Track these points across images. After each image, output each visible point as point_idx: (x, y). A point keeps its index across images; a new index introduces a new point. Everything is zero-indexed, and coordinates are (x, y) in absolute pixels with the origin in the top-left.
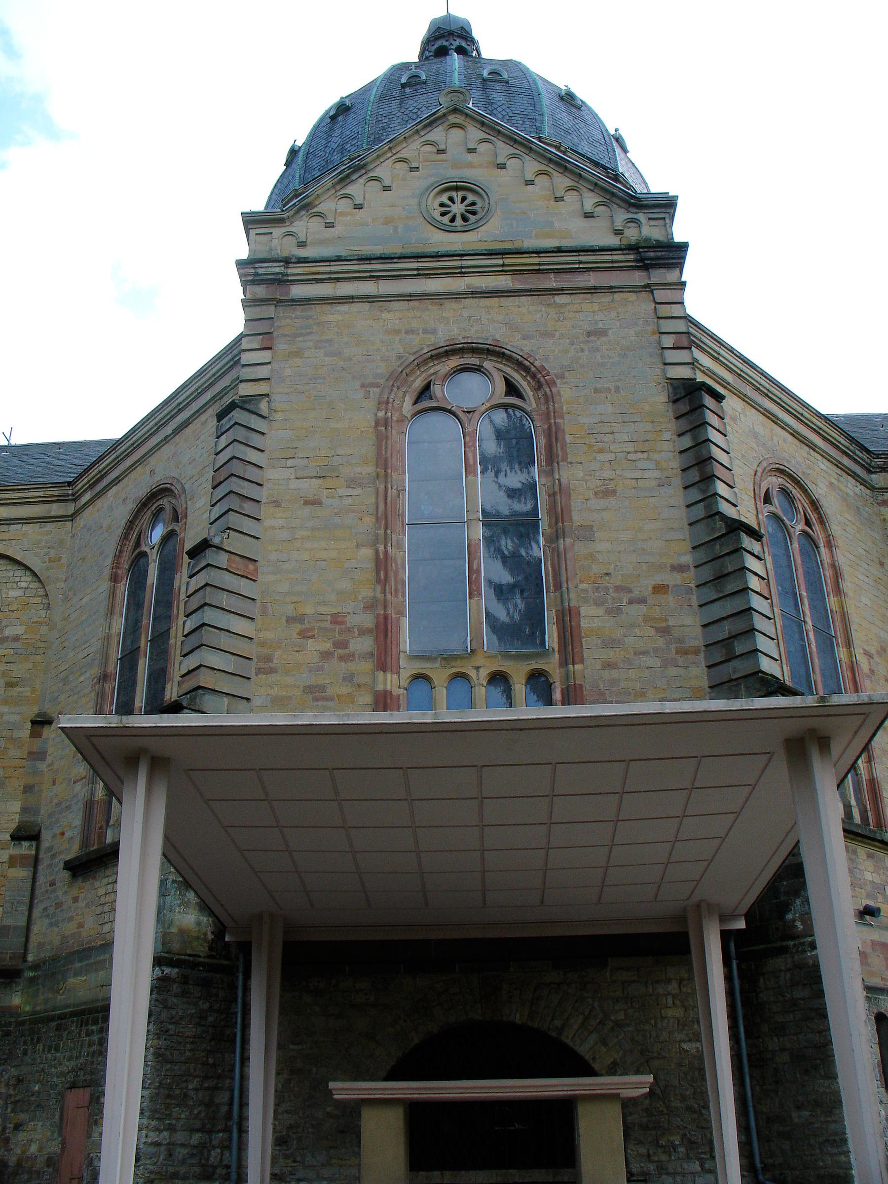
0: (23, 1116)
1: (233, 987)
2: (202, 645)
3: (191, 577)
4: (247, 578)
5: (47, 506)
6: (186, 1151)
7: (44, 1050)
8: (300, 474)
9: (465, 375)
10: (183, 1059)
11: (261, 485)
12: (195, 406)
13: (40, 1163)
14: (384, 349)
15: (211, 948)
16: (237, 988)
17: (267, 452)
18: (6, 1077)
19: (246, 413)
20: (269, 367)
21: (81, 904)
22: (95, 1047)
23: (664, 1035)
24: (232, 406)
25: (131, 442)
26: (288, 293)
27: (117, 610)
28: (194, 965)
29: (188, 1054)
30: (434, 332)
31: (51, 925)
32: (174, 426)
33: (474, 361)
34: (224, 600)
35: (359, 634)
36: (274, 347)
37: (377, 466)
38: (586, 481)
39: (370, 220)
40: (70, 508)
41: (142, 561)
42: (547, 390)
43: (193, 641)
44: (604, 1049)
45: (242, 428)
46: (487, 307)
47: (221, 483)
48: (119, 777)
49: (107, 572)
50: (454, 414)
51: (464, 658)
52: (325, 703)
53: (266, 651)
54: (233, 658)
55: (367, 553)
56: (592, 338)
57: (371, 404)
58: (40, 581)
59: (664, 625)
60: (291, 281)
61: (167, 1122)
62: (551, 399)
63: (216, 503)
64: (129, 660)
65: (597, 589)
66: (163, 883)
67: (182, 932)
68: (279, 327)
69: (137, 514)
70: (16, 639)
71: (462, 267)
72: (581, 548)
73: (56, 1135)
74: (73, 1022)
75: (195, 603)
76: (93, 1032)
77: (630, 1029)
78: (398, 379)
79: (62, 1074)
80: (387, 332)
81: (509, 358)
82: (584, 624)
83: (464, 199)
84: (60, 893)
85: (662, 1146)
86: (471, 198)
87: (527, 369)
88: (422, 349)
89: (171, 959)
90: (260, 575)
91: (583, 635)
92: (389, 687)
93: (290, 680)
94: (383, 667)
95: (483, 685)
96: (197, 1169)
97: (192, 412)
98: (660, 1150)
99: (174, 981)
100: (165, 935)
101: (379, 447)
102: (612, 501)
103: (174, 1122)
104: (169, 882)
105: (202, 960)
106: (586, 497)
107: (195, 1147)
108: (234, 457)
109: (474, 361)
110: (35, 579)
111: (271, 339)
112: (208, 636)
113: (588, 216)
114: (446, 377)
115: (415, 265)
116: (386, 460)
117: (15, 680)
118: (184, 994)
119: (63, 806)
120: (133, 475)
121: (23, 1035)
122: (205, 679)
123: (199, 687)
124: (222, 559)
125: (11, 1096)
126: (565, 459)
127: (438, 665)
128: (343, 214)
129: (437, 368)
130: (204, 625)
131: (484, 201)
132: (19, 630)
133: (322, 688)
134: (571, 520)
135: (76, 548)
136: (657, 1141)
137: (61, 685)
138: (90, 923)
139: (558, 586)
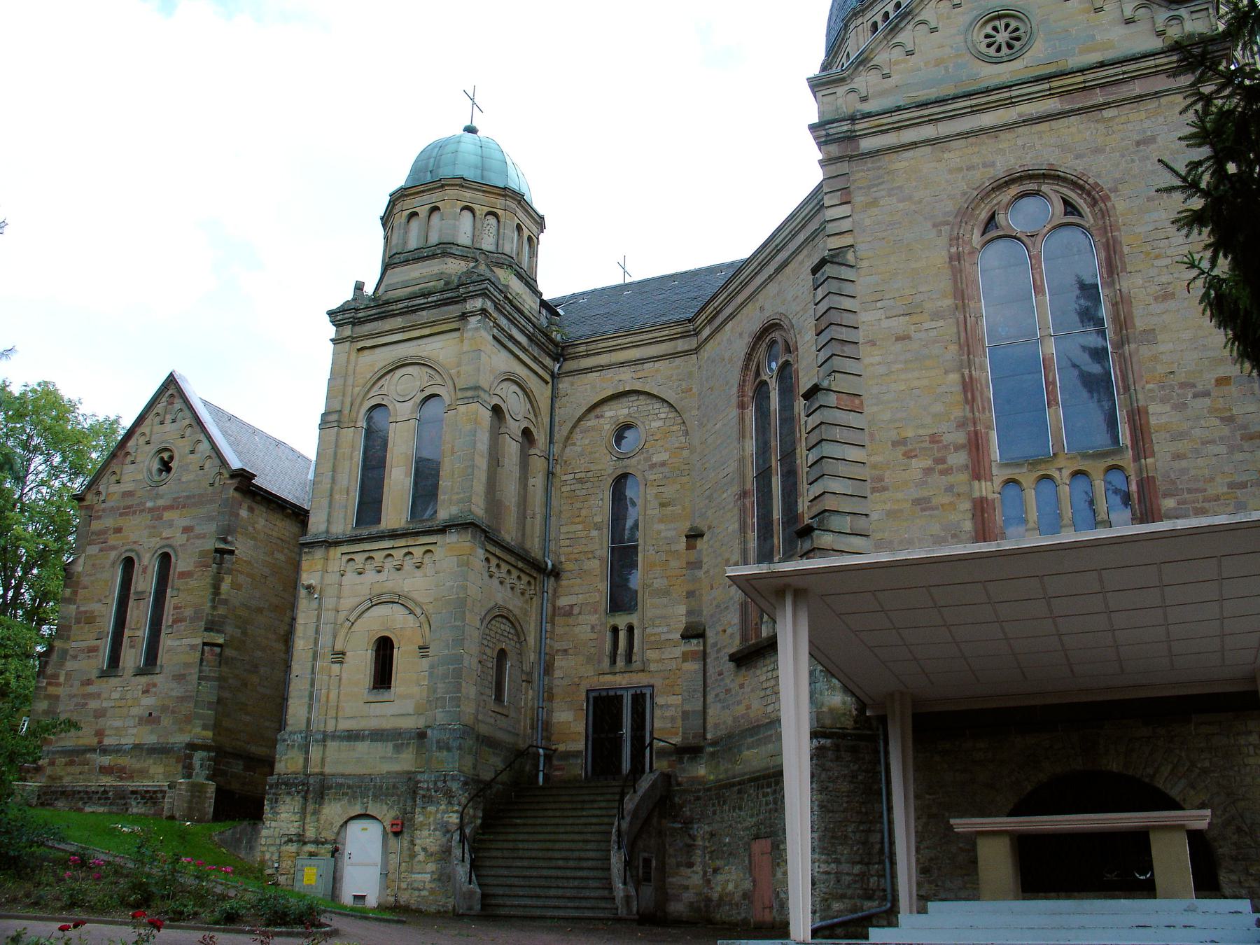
0: (719, 863)
1: (877, 752)
2: (824, 475)
3: (808, 416)
4: (855, 411)
5: (673, 343)
6: (851, 878)
7: (729, 810)
8: (889, 314)
9: (1025, 200)
10: (842, 809)
11: (857, 328)
12: (792, 247)
13: (737, 898)
14: (950, 188)
15: (856, 722)
16: (879, 752)
17: (858, 297)
18: (701, 832)
19: (836, 266)
20: (850, 219)
21: (747, 689)
22: (771, 806)
23: (1248, 780)
24: (823, 262)
25: (739, 281)
26: (858, 148)
27: (748, 434)
28: (843, 736)
29: (845, 805)
30: (993, 164)
31: (723, 708)
32: (776, 266)
33: (1032, 186)
34: (838, 434)
35: (955, 450)
36: (853, 201)
37: (955, 298)
38: (1145, 288)
39: (922, 64)
40: (693, 342)
41: (764, 389)
42: (1103, 205)
43: (815, 472)
44: (1192, 792)
45: (833, 280)
46: (1039, 132)
47: (822, 331)
48: (772, 604)
49: (734, 400)
50: (1019, 239)
51: (1048, 461)
52: (931, 512)
53: (877, 472)
54: (850, 482)
55: (954, 377)
56: (1142, 147)
57: (943, 241)
58: (676, 411)
59: (1228, 414)
60: (860, 135)
61: (833, 857)
62: (1106, 214)
63: (821, 349)
64: (764, 476)
65: (1163, 387)
66: (812, 673)
67: (831, 710)
68: (855, 181)
69: (753, 347)
70: (663, 464)
71: (1011, 98)
72: (1145, 351)
73: (747, 875)
74: (751, 787)
75: (814, 438)
76: (768, 794)
77: (1216, 775)
78: (965, 214)
79: (747, 828)
80: (950, 171)
81: (1065, 180)
82: (1153, 421)
83: (1007, 26)
84: (728, 681)
85: (1252, 875)
86: (1013, 24)
87: (1082, 188)
88: (984, 183)
89: (825, 733)
90: (865, 408)
91: (1153, 431)
92: (984, 494)
93: (900, 495)
94: (977, 476)
95: (1066, 484)
96: (860, 892)
97: (790, 252)
98: (1250, 878)
99: (828, 749)
100: (818, 714)
101: (955, 282)
102: (1171, 304)
103: (839, 856)
104: (818, 672)
105: (849, 731)
106: (1147, 303)
107: (857, 875)
108: (830, 308)
109: (1032, 186)
110: (672, 410)
111: (849, 193)
112: (828, 466)
113: (1129, 21)
114: (1007, 207)
115: (969, 103)
116: (962, 291)
117: (667, 500)
118: (838, 759)
119: (722, 607)
120: (745, 311)
121: (711, 799)
122: (830, 503)
123: (826, 511)
124: (832, 399)
125: (707, 847)
126: (1124, 269)
127: (1025, 470)
128: (897, 63)
129: (1000, 198)
130: (823, 457)
131: (1026, 24)
132: (664, 456)
133: (927, 500)
134: (1134, 326)
135: (704, 379)
136: (1248, 871)
137: (707, 501)
138: (756, 705)
139: (1127, 389)
